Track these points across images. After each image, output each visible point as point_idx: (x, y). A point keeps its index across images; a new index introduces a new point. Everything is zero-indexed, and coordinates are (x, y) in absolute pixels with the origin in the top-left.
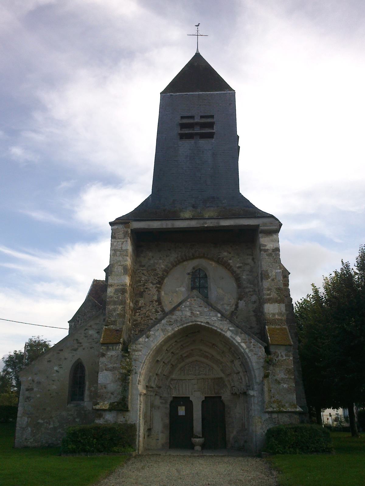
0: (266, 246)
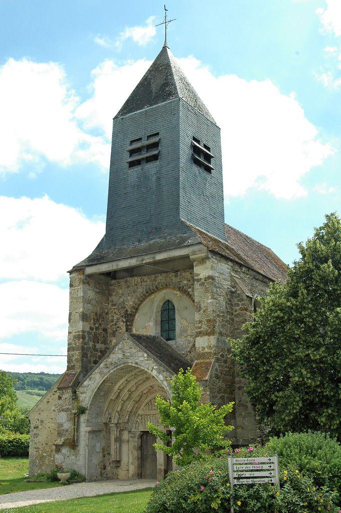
0: (198, 275)
